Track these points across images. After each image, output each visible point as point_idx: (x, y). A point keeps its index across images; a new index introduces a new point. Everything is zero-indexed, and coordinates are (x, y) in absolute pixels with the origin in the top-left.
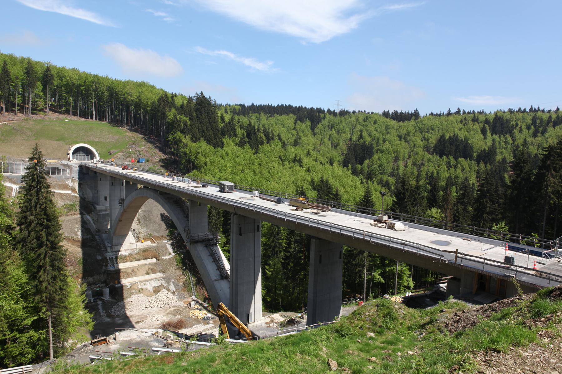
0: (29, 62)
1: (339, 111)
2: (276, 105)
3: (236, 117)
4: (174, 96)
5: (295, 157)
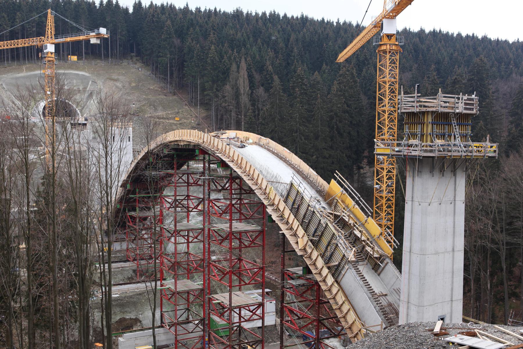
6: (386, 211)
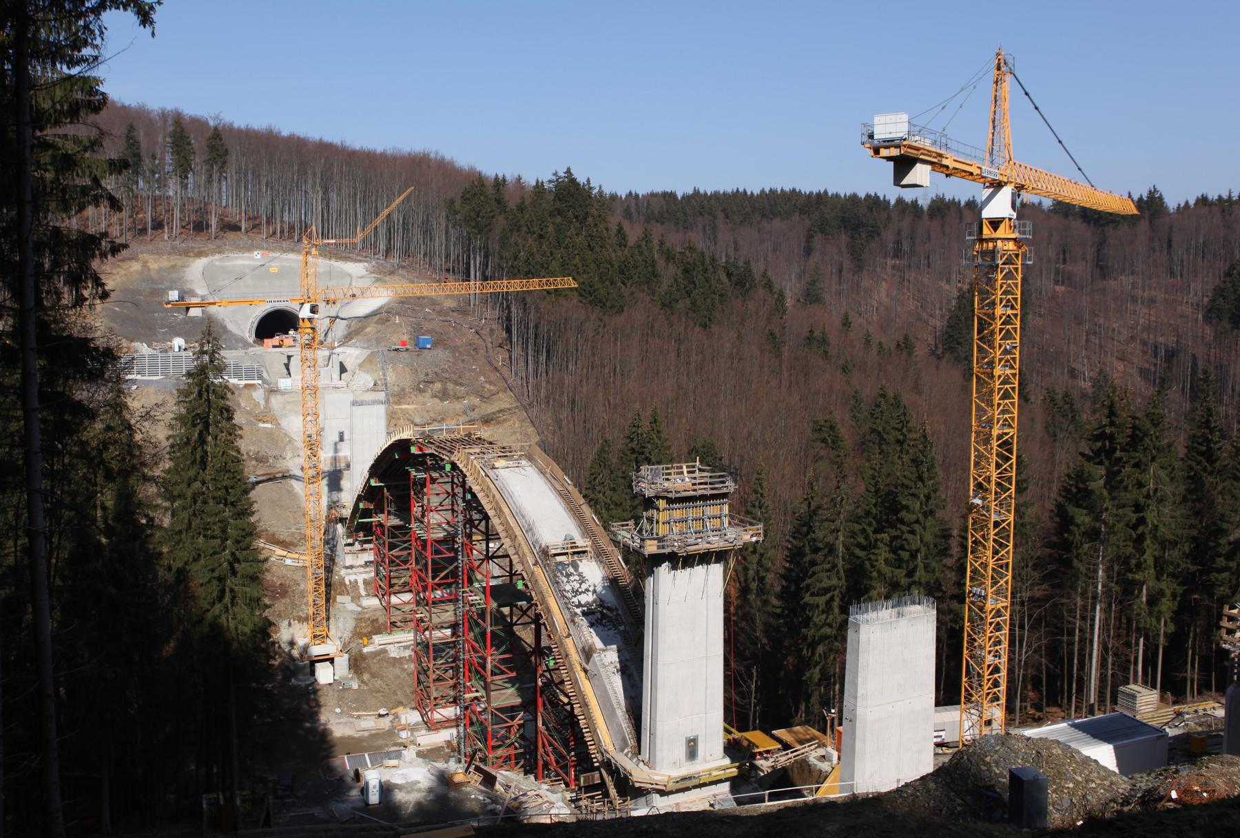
0: (178, 119)
1: (929, 202)
2: (756, 192)
3: (657, 230)
4: (499, 184)
5: (811, 332)
6: (999, 405)
